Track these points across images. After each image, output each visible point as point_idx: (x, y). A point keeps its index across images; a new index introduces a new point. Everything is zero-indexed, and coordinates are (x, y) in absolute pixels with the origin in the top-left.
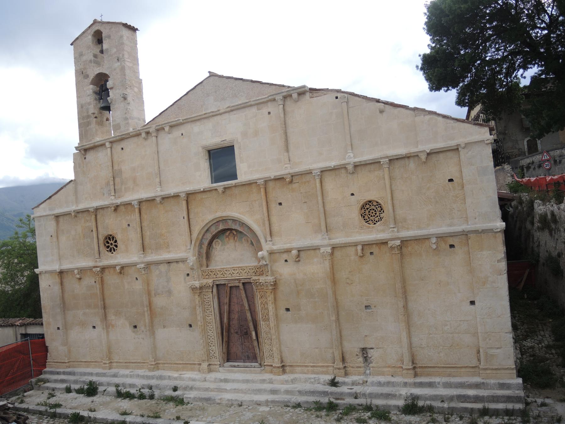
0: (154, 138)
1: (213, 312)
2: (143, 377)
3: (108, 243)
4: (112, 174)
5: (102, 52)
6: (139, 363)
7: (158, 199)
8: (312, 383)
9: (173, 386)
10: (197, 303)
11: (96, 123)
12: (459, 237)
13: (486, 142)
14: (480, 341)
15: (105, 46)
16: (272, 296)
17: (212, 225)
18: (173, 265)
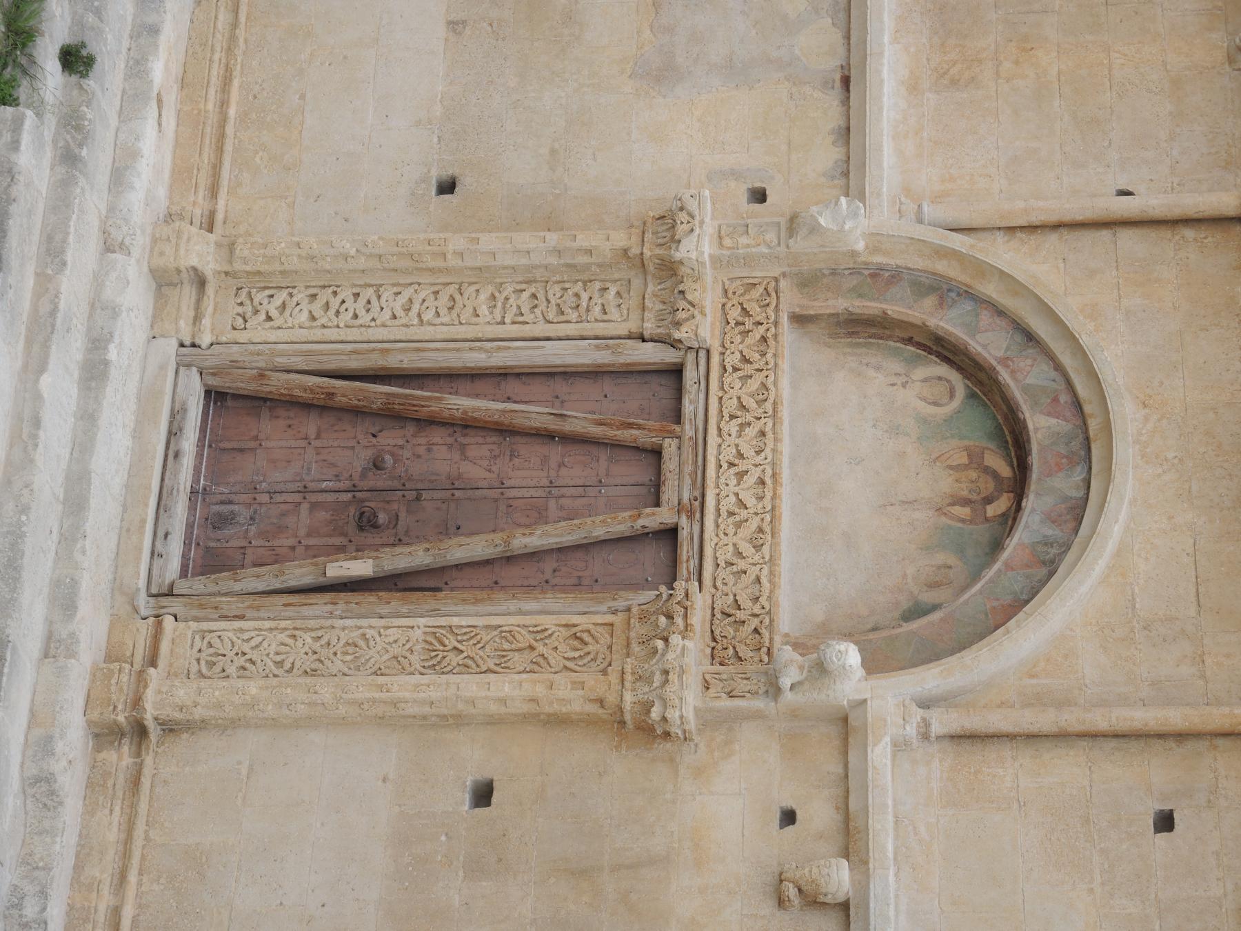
1: (514, 331)
9: (93, 48)
10: (583, 240)
16: (577, 705)
17: (1058, 367)
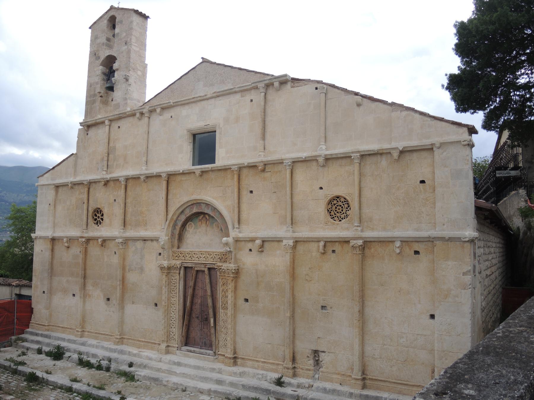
0: (146, 119)
2: (106, 349)
3: (96, 215)
4: (107, 150)
5: (114, 36)
6: (107, 335)
7: (142, 178)
8: (259, 379)
9: (129, 362)
10: (164, 282)
11: (100, 102)
12: (424, 243)
13: (463, 143)
14: (436, 360)
15: (117, 30)
17: (187, 207)
18: (149, 243)
